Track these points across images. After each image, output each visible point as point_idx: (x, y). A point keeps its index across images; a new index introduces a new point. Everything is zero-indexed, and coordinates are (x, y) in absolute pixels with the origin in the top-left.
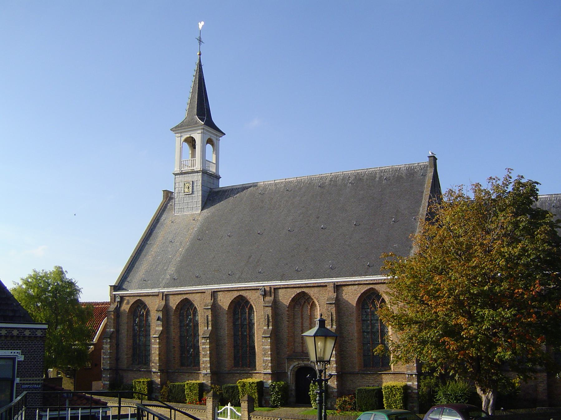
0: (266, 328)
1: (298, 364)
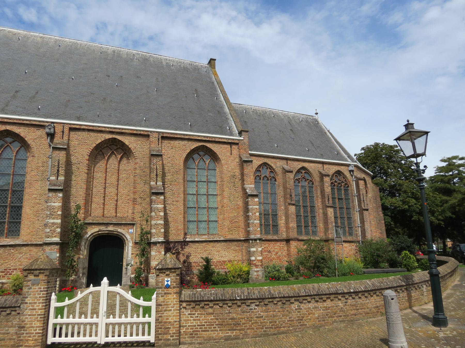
1: (99, 231)
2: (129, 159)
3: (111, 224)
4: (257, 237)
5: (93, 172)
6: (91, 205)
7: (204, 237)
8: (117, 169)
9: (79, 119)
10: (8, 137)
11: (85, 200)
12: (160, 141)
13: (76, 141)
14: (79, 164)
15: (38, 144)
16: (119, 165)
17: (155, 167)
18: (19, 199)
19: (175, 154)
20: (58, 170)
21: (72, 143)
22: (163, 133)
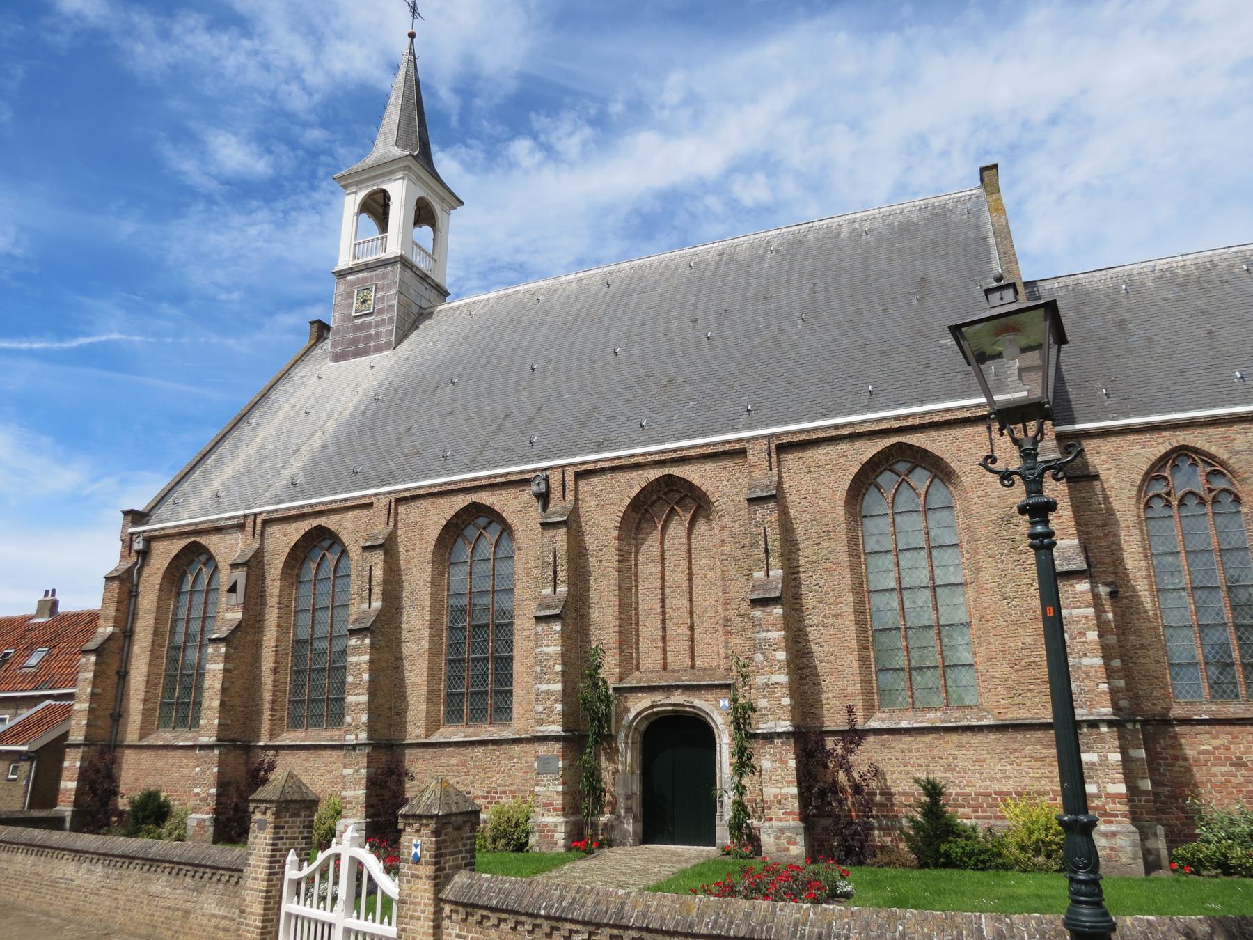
0: (548, 591)
1: (652, 707)
2: (711, 520)
3: (678, 687)
4: (1098, 714)
5: (636, 565)
6: (637, 644)
7: (931, 715)
8: (685, 547)
9: (599, 448)
10: (480, 516)
11: (620, 632)
12: (774, 459)
13: (591, 499)
14: (602, 551)
15: (524, 520)
16: (689, 539)
17: (761, 531)
18: (507, 642)
19: (819, 484)
20: (555, 573)
21: (584, 506)
22: (779, 435)
